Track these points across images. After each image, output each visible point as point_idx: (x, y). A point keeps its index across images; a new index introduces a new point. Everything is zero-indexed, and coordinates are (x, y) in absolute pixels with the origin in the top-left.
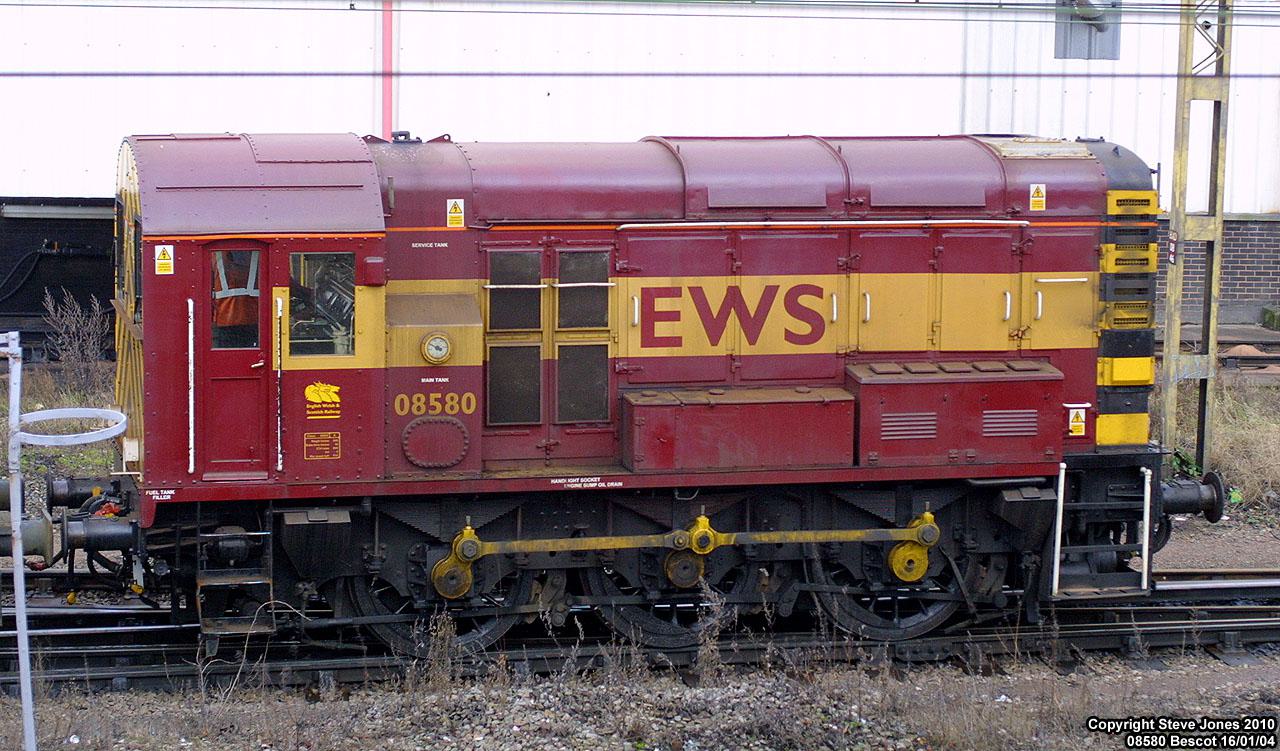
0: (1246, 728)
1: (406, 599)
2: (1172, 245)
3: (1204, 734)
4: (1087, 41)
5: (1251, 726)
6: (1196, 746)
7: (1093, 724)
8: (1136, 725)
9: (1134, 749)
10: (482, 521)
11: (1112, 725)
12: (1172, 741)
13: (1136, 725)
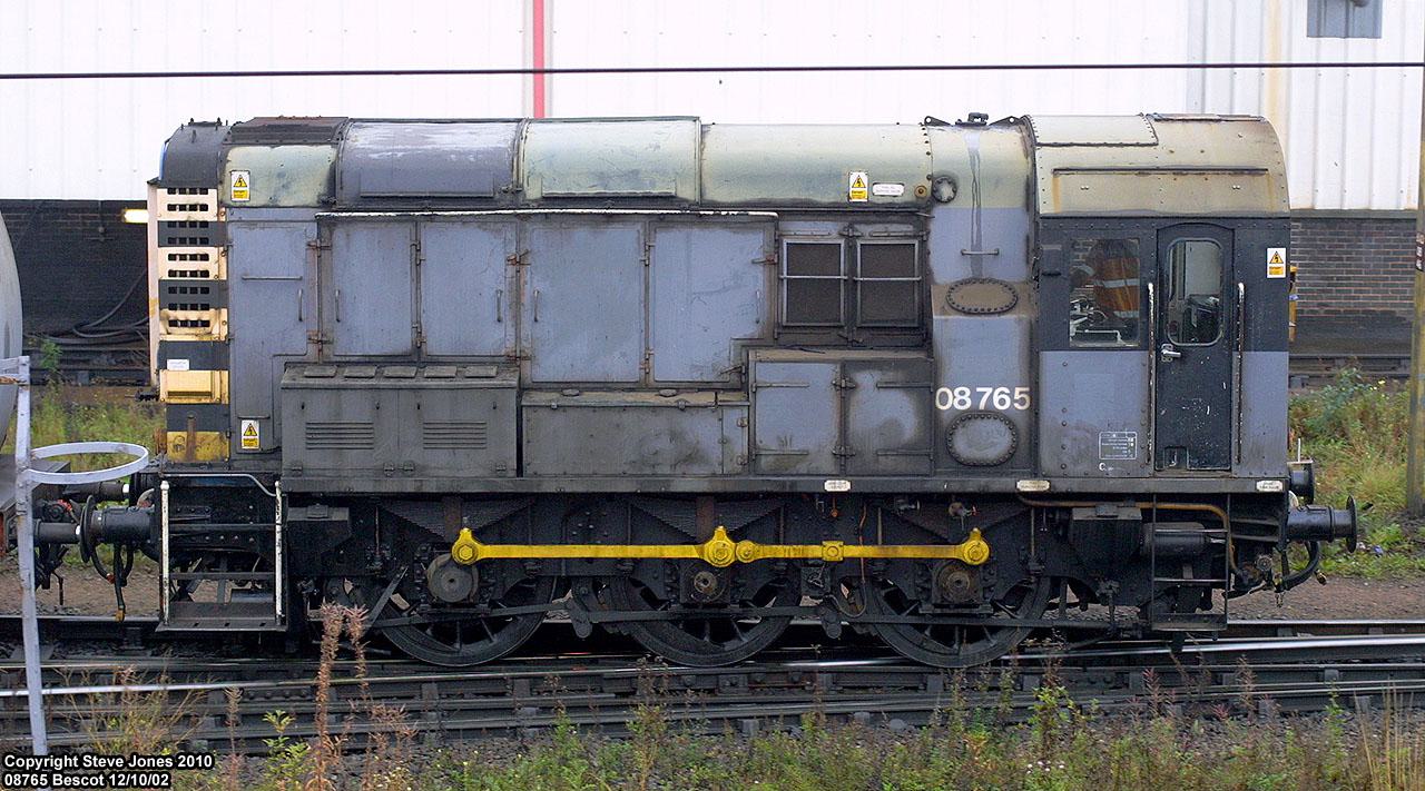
0: (180, 765)
1: (913, 602)
2: (1420, 249)
3: (90, 772)
4: (1343, 17)
5: (185, 763)
6: (81, 785)
7: (10, 761)
8: (58, 762)
9: (160, 789)
10: (987, 523)
11: (30, 762)
12: (55, 780)
13: (58, 762)
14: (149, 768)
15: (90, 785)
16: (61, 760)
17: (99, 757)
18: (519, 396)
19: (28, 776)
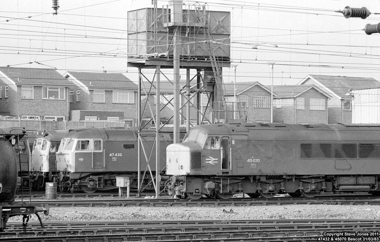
0: (371, 235)
5: (372, 234)
7: (325, 234)
8: (338, 234)
11: (330, 234)
13: (338, 234)
14: (362, 236)
15: (358, 240)
16: (339, 234)
17: (349, 233)
18: (232, 111)
19: (343, 238)
